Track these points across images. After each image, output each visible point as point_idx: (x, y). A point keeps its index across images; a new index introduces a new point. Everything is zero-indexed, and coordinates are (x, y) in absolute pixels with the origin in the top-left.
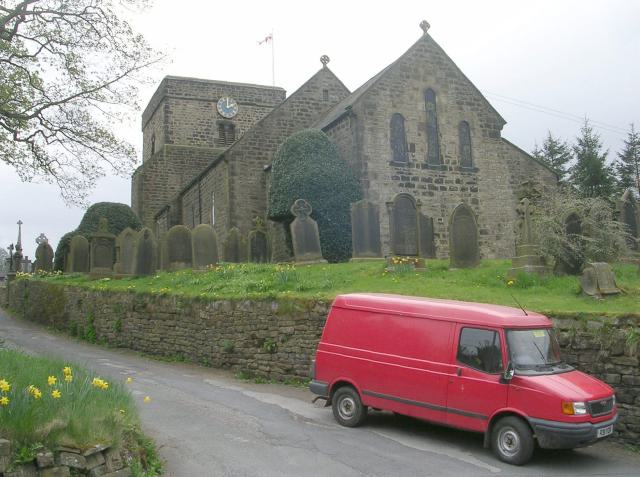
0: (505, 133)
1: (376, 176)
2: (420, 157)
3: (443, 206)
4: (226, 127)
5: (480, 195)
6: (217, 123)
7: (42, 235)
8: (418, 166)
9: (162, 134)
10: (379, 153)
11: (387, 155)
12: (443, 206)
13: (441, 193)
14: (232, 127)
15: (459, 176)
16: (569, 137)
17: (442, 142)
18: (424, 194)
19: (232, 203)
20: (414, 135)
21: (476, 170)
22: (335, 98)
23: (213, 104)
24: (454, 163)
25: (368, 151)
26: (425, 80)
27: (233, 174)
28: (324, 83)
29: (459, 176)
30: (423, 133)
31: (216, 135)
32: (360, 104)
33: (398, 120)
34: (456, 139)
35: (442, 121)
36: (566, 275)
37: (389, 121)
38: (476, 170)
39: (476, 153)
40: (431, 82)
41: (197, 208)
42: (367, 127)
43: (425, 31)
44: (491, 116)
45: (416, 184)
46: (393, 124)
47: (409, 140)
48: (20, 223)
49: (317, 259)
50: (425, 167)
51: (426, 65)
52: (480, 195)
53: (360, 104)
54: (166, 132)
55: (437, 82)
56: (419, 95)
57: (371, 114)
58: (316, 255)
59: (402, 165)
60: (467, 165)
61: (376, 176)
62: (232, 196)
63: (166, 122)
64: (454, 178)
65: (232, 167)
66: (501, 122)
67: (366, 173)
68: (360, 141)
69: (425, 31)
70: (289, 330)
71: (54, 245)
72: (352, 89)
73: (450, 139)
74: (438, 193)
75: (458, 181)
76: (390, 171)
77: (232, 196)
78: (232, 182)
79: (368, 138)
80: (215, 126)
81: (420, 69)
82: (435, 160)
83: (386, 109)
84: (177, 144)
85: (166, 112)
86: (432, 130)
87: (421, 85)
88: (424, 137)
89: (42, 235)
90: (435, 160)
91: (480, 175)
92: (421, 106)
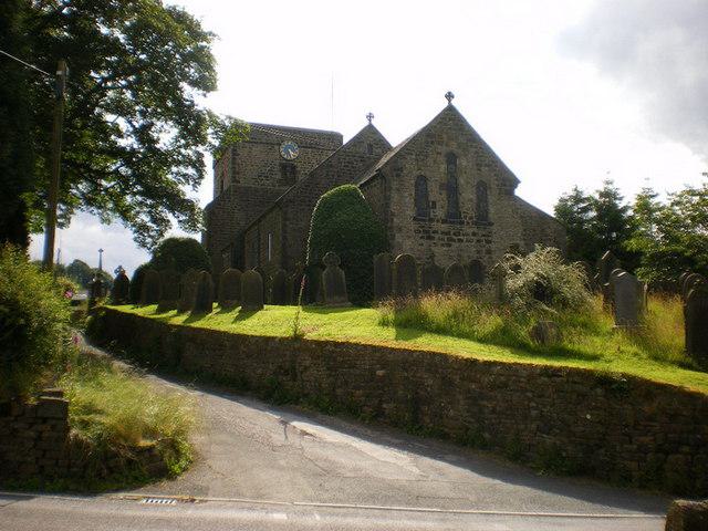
0: (518, 192)
1: (400, 230)
2: (440, 213)
3: (459, 255)
4: (288, 168)
5: (493, 246)
6: (280, 164)
7: (120, 267)
8: (438, 221)
9: (230, 175)
10: (403, 207)
11: (411, 212)
12: (459, 255)
13: (458, 245)
14: (294, 168)
15: (475, 230)
16: (591, 190)
17: (461, 200)
18: (443, 245)
19: (284, 245)
20: (436, 194)
21: (491, 224)
22: (379, 151)
23: (276, 147)
24: (471, 218)
25: (394, 208)
26: (447, 145)
27: (285, 219)
28: (370, 139)
29: (475, 230)
30: (444, 192)
31: (279, 176)
32: (388, 167)
33: (422, 181)
34: (473, 197)
35: (462, 181)
36: (121, 429)
37: (413, 182)
38: (491, 224)
39: (492, 210)
40: (454, 147)
41: (256, 246)
42: (394, 187)
43: (450, 101)
44: (174, 330)
45: (437, 236)
46: (417, 185)
47: (431, 198)
48: (101, 251)
49: (343, 302)
50: (444, 222)
51: (449, 131)
52: (493, 246)
53: (388, 167)
54: (234, 173)
55: (459, 146)
56: (442, 159)
57: (398, 175)
58: (342, 298)
59: (424, 220)
60: (482, 219)
61: (400, 230)
62: (285, 238)
63: (233, 163)
64: (470, 231)
65: (286, 213)
66: (514, 182)
67: (391, 228)
68: (387, 198)
69: (450, 101)
70: (308, 363)
71: (130, 275)
72: (394, 144)
73: (468, 196)
74: (455, 245)
75: (474, 234)
76: (413, 226)
77: (285, 238)
78: (285, 225)
79: (395, 197)
80: (277, 168)
81: (445, 136)
82: (454, 216)
83: (410, 166)
84: (243, 183)
85: (234, 154)
86: (452, 189)
87: (443, 149)
88: (444, 196)
89: (120, 267)
90: (454, 216)
91: (494, 228)
92: (443, 167)
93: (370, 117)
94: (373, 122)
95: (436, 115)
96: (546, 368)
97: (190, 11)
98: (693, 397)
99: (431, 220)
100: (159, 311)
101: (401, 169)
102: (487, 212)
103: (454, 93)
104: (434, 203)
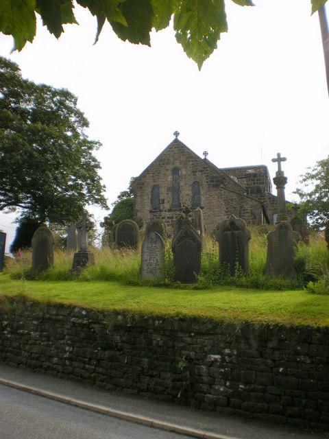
17: (181, 195)
20: (164, 194)
30: (170, 193)
33: (156, 187)
34: (189, 192)
35: (182, 184)
39: (203, 198)
43: (177, 137)
50: (169, 211)
56: (169, 173)
57: (141, 188)
69: (177, 137)
81: (171, 159)
86: (175, 190)
87: (170, 167)
92: (170, 178)
93: (177, 134)
94: (179, 138)
95: (183, 142)
96: (181, 425)
97: (48, 84)
98: (304, 335)
99: (161, 211)
100: (102, 201)
101: (143, 184)
102: (199, 201)
103: (179, 131)
104: (163, 201)
